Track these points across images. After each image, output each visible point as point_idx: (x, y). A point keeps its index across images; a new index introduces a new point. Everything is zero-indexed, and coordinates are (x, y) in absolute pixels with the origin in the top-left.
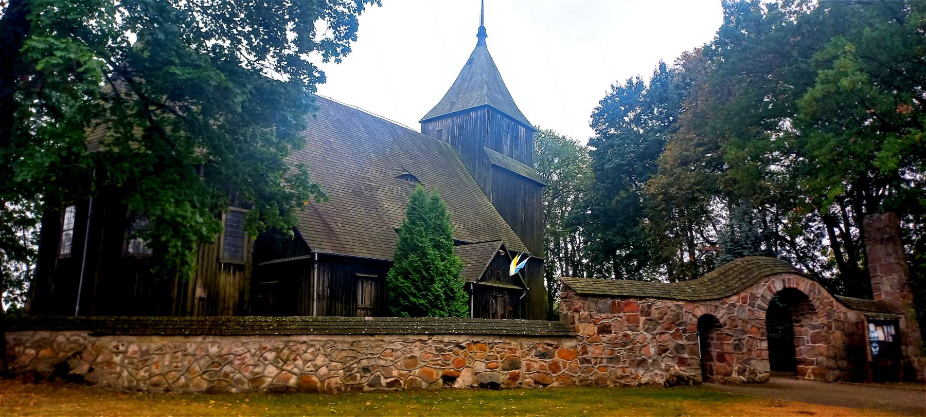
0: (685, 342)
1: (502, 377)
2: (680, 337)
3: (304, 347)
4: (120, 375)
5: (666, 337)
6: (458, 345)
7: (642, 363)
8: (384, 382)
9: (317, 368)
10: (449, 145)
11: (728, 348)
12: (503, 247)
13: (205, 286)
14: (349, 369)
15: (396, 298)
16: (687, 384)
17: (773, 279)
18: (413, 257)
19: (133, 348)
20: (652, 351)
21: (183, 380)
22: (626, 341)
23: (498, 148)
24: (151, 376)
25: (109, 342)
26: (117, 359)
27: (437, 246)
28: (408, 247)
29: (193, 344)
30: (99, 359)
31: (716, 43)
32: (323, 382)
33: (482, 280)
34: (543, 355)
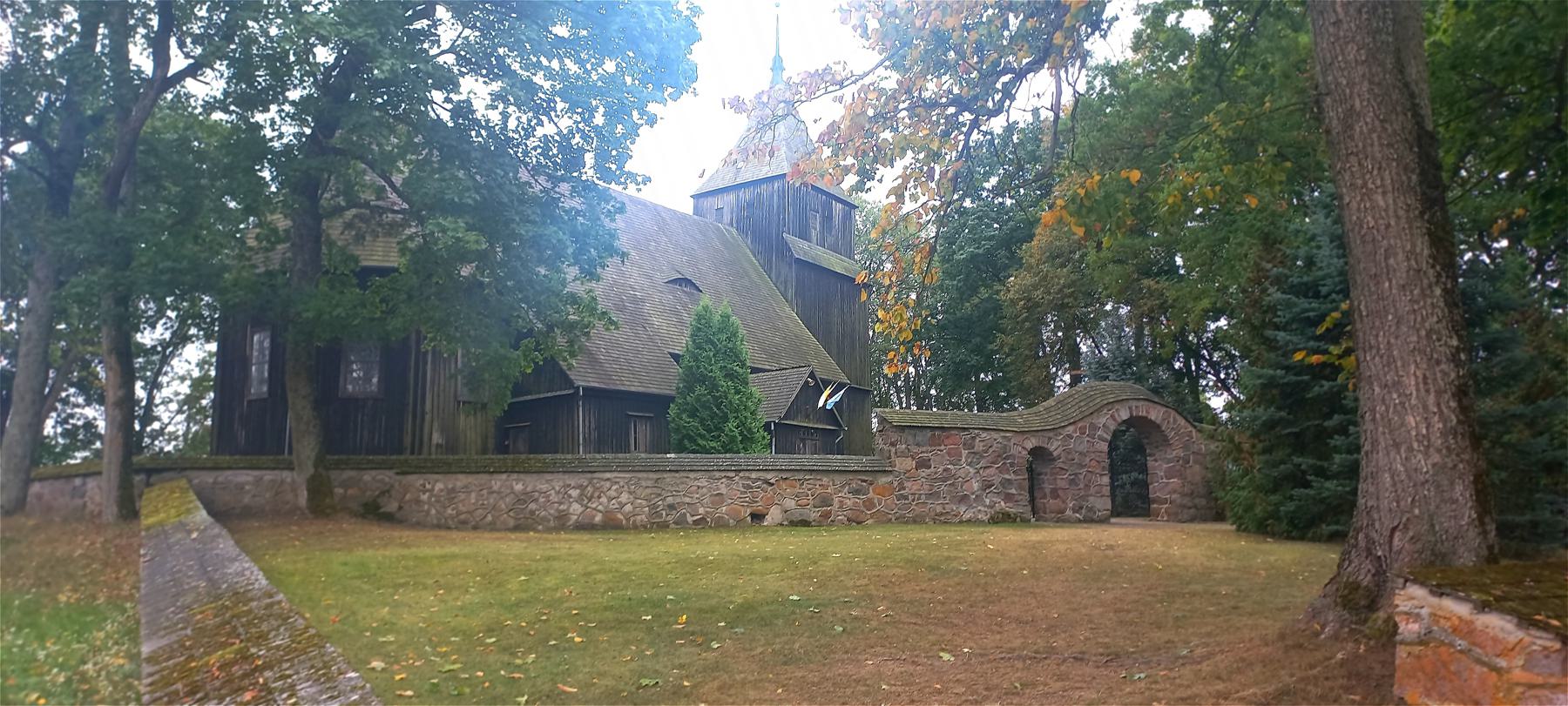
0: (1012, 477)
1: (813, 515)
2: (1008, 472)
3: (608, 484)
4: (428, 512)
5: (991, 471)
7: (964, 499)
8: (690, 519)
9: (622, 505)
10: (734, 231)
11: (1061, 484)
12: (812, 375)
13: (442, 430)
14: (655, 506)
15: (681, 441)
16: (1015, 521)
17: (1117, 406)
18: (700, 390)
19: (439, 486)
20: (976, 486)
21: (489, 518)
22: (947, 476)
23: (805, 236)
25: (417, 480)
26: (425, 497)
27: (730, 375)
28: (693, 378)
29: (497, 482)
30: (408, 497)
32: (628, 520)
33: (786, 417)
34: (856, 492)
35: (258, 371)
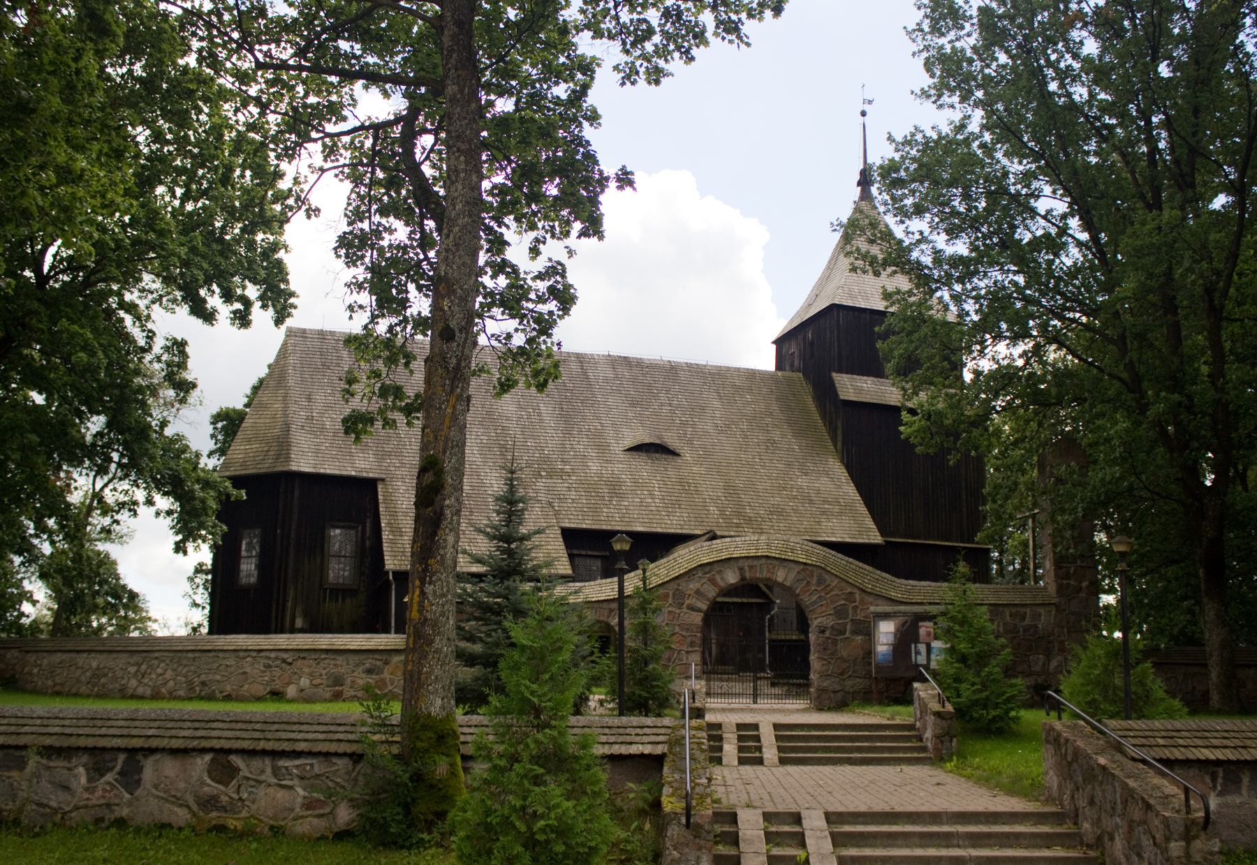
3: (156, 662)
6: (284, 661)
19: (45, 662)
24: (55, 685)
26: (35, 671)
31: (597, 195)
34: (369, 671)
35: (248, 568)
